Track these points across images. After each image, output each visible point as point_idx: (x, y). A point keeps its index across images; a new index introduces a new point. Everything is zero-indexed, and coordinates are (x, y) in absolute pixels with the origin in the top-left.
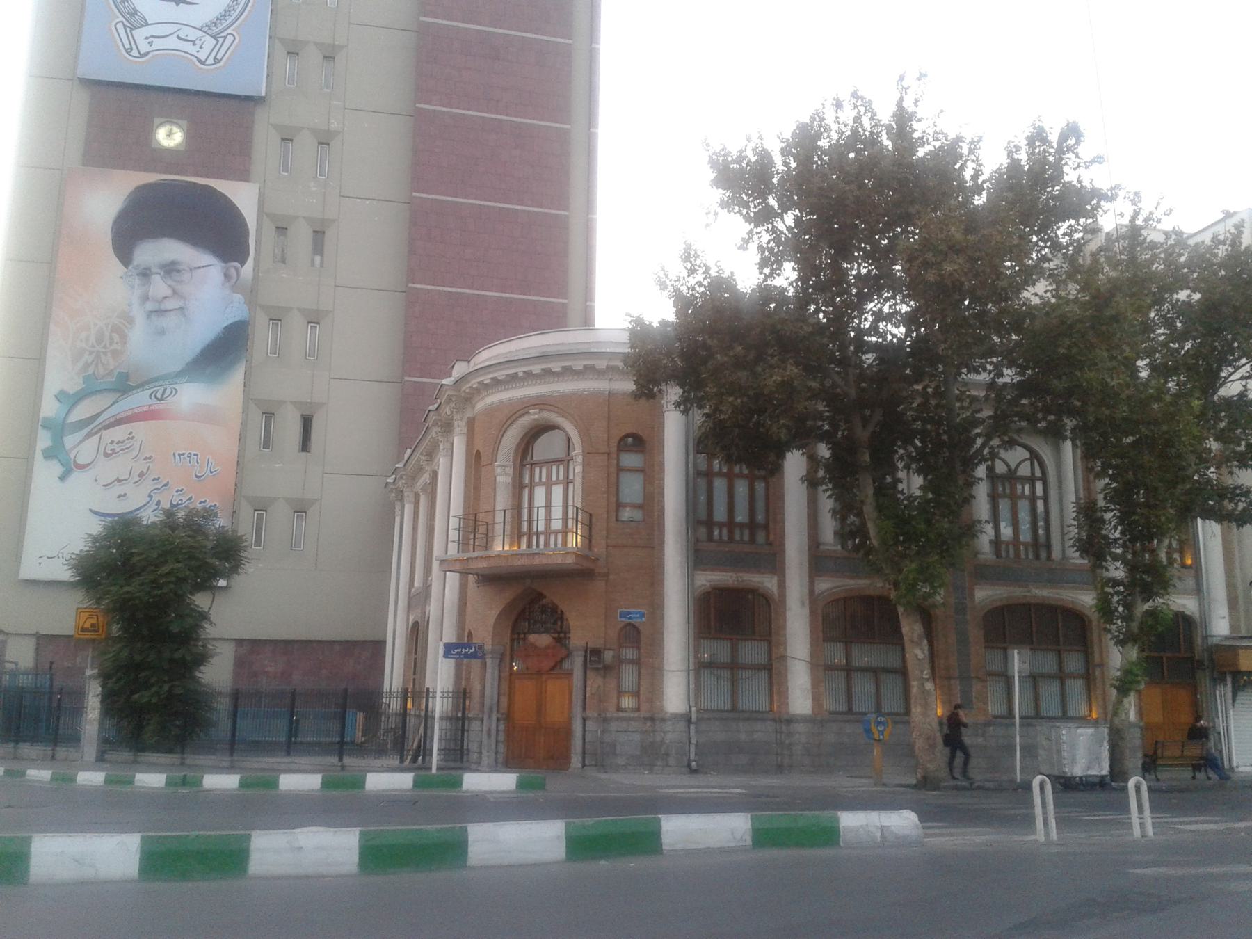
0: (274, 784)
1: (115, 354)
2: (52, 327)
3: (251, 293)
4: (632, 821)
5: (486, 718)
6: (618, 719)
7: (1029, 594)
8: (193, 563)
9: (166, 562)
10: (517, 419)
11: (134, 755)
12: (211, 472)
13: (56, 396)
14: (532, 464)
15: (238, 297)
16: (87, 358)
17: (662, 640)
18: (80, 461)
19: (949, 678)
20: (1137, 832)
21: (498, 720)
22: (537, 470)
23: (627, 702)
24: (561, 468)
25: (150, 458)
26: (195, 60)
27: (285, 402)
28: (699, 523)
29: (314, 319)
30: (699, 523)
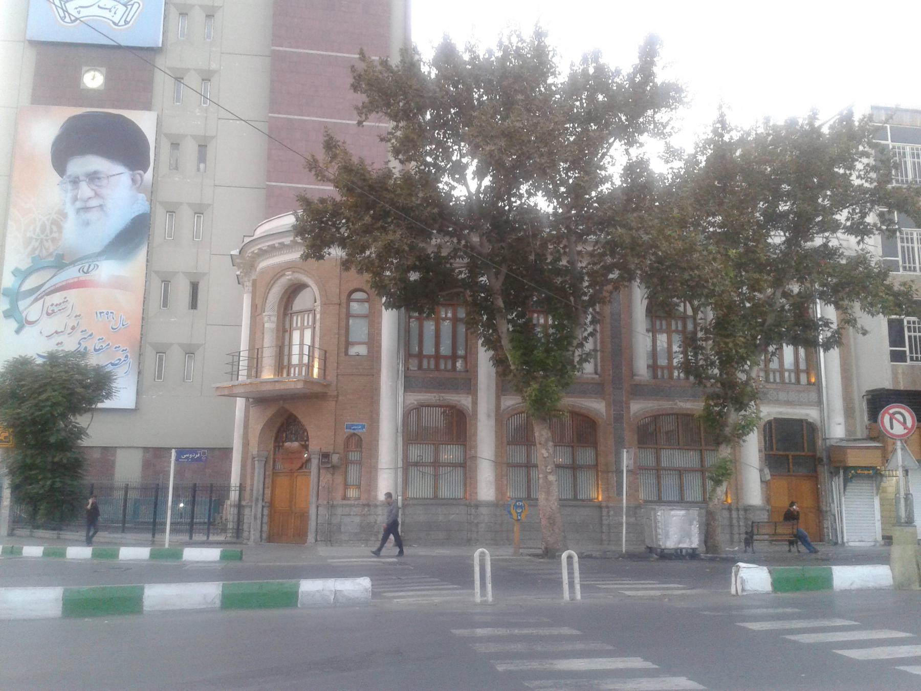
0: (115, 555)
1: (54, 240)
2: (10, 223)
3: (152, 193)
4: (275, 583)
5: (253, 506)
6: (342, 506)
7: (675, 407)
8: (66, 392)
9: (45, 391)
10: (277, 279)
11: (30, 531)
12: (123, 325)
13: (12, 273)
15: (142, 196)
16: (35, 244)
18: (30, 319)
19: (608, 472)
20: (566, 595)
21: (263, 507)
22: (295, 318)
25: (79, 316)
26: (111, 23)
29: (199, 211)
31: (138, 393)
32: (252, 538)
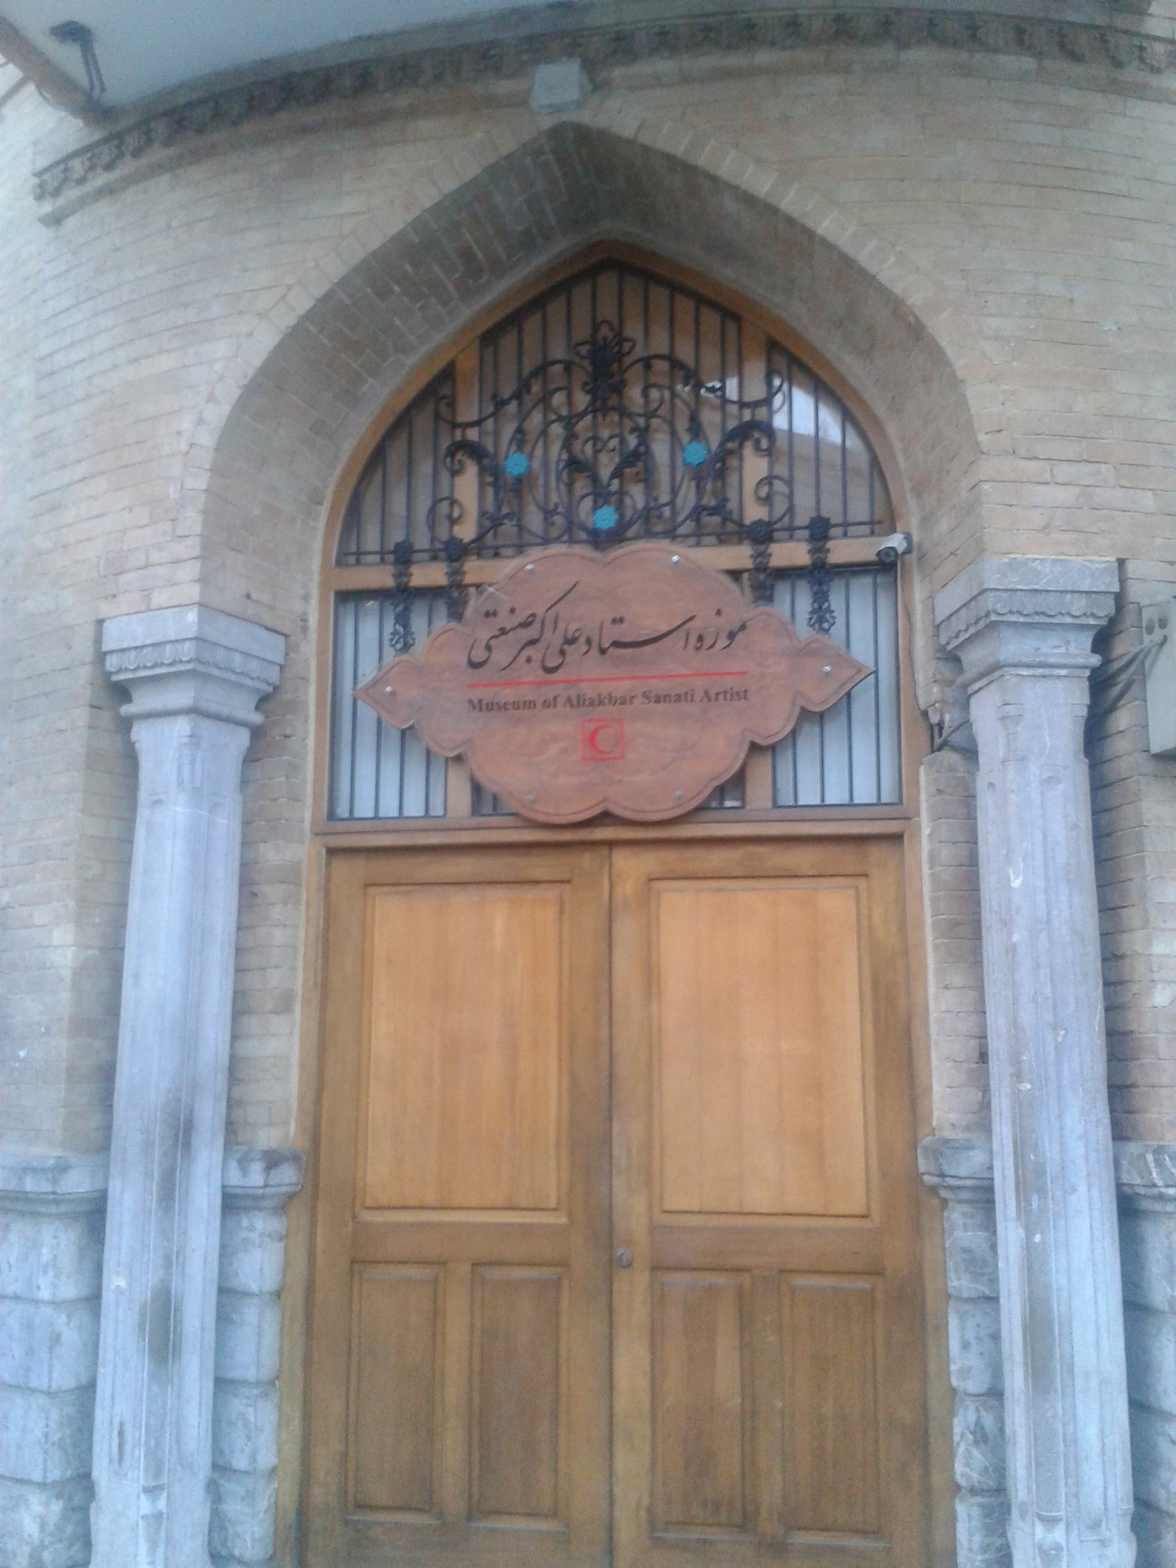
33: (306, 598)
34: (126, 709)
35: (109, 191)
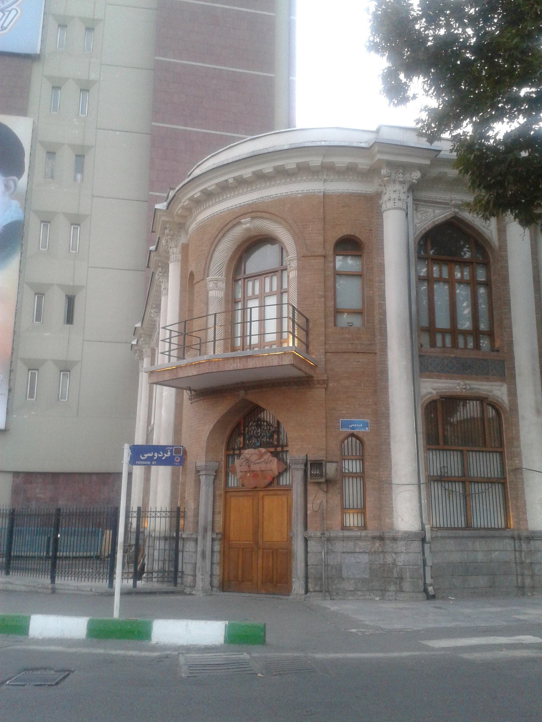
5: (200, 538)
6: (344, 539)
10: (228, 231)
14: (245, 279)
17: (389, 451)
21: (213, 540)
22: (250, 284)
23: (352, 520)
24: (275, 279)
27: (52, 285)
28: (423, 330)
30: (423, 330)
31: (8, 412)
32: (199, 584)
33: (222, 456)
34: (199, 474)
35: (196, 401)
